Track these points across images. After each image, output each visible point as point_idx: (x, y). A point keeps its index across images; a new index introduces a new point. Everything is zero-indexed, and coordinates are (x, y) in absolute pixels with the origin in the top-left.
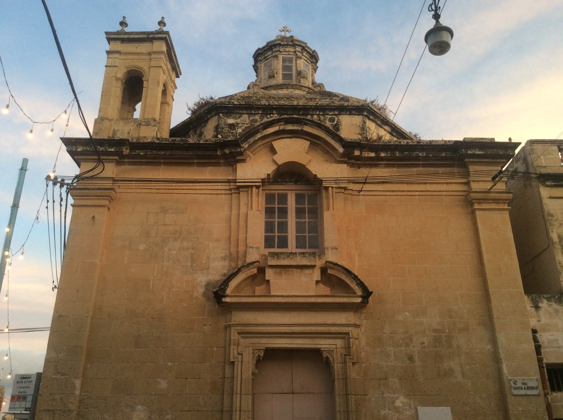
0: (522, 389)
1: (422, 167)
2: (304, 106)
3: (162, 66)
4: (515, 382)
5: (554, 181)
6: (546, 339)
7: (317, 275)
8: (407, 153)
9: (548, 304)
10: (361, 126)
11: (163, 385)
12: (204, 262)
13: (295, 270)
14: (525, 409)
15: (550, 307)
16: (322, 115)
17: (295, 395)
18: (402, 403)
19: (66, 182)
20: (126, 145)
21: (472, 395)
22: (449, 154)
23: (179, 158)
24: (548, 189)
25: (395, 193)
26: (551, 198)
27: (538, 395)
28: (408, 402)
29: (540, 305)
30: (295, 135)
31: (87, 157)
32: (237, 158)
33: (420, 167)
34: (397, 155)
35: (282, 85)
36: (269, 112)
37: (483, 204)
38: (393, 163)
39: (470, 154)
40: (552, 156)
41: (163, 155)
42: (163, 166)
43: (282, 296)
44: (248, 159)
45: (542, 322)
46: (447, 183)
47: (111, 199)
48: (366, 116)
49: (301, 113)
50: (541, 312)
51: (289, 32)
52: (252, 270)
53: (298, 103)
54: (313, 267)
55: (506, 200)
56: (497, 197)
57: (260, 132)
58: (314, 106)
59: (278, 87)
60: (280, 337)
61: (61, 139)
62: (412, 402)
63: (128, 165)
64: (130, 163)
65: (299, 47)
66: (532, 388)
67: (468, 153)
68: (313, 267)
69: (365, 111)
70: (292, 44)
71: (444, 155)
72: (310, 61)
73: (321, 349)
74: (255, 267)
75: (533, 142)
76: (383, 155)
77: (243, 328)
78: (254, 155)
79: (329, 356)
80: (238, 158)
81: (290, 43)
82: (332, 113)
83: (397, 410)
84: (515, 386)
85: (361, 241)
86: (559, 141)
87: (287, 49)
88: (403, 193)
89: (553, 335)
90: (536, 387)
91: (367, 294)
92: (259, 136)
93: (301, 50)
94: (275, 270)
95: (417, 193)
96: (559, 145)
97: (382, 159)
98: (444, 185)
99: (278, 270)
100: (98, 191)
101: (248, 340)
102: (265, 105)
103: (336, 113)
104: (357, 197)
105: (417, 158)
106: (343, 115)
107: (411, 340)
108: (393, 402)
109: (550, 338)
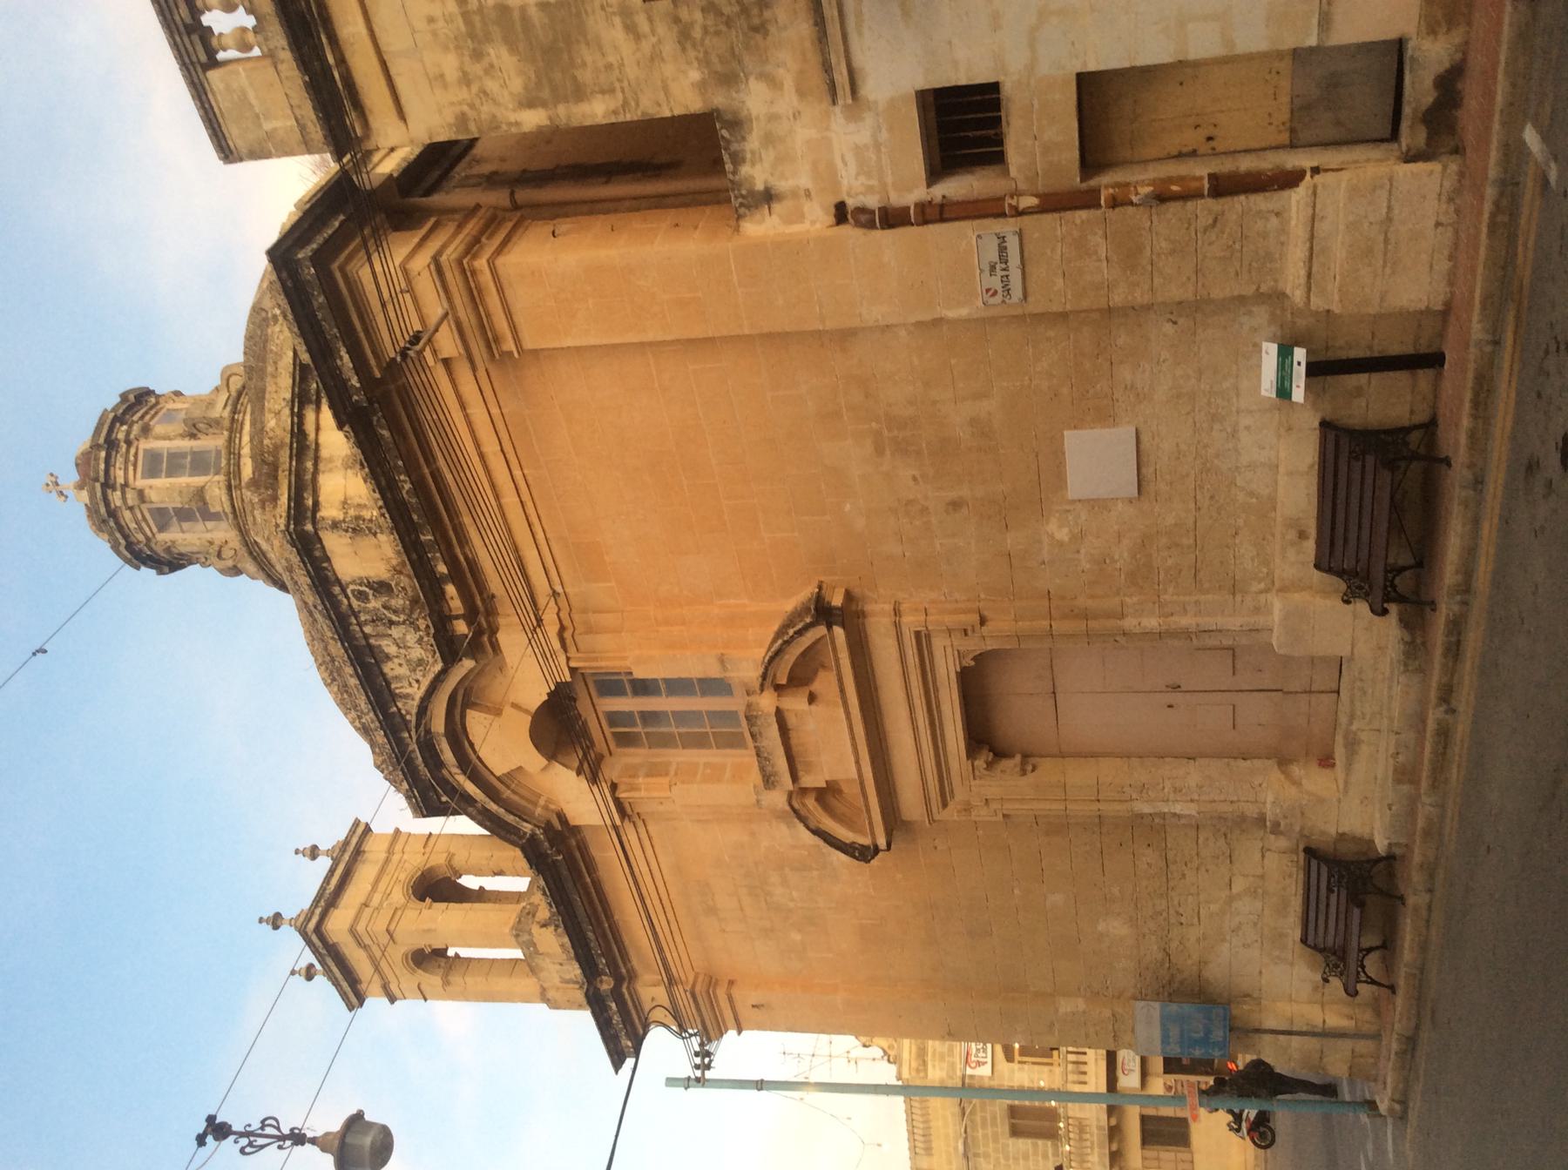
0: (1007, 276)
1: (435, 460)
3: (387, 930)
6: (856, 179)
7: (795, 704)
8: (415, 517)
9: (753, 164)
10: (349, 534)
11: (1057, 899)
14: (1060, 272)
15: (761, 159)
16: (357, 618)
18: (1060, 527)
19: (697, 1049)
20: (595, 988)
23: (591, 902)
24: (375, 123)
27: (1020, 234)
29: (760, 186)
32: (560, 828)
35: (255, 559)
36: (398, 719)
37: (497, 326)
38: (451, 533)
39: (360, 381)
40: (251, 95)
41: (595, 933)
42: (616, 917)
44: (552, 807)
47: (712, 982)
48: (314, 523)
49: (373, 661)
50: (781, 185)
54: (779, 713)
56: (465, 299)
61: (617, 1072)
63: (630, 962)
64: (625, 958)
66: (1002, 249)
67: (358, 385)
69: (303, 530)
71: (386, 433)
72: (128, 451)
73: (959, 670)
74: (804, 805)
76: (442, 568)
77: (934, 802)
78: (540, 796)
79: (971, 656)
82: (341, 597)
83: (1079, 537)
84: (1000, 291)
87: (133, 525)
88: (529, 505)
91: (822, 612)
92: (493, 807)
94: (801, 773)
95: (517, 473)
97: (452, 562)
98: (503, 501)
99: (799, 767)
100: (703, 1009)
102: (386, 735)
103: (337, 590)
105: (419, 487)
106: (335, 574)
107: (909, 502)
108: (1061, 544)
109: (853, 167)
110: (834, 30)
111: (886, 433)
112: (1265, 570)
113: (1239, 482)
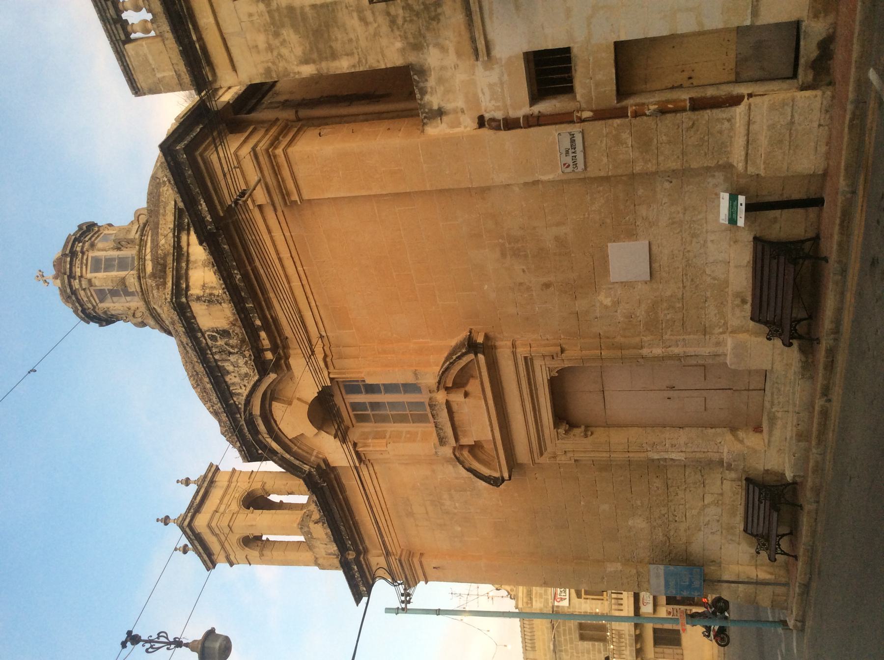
2: (208, 376)
4: (566, 166)
5: (200, 68)
7: (457, 398)
8: (243, 294)
9: (432, 94)
11: (605, 507)
12: (463, 481)
13: (456, 419)
17: (606, 389)
18: (606, 297)
21: (589, 215)
22: (221, 239)
25: (305, 282)
26: (234, 68)
27: (583, 133)
28: (604, 291)
29: (435, 107)
30: (269, 415)
31: (358, 539)
33: (255, 266)
34: (251, 305)
39: (211, 218)
40: (150, 58)
43: (492, 431)
44: (321, 456)
45: (464, 107)
46: (269, 232)
47: (411, 554)
48: (187, 297)
49: (220, 374)
50: (448, 106)
51: (43, 273)
52: (466, 456)
53: (208, 383)
54: (448, 404)
55: (269, 156)
57: (282, 456)
58: (203, 365)
59: (159, 320)
60: (540, 418)
62: (604, 287)
65: (73, 284)
66: (573, 141)
68: (448, 404)
70: (73, 296)
71: (226, 247)
75: (135, 90)
76: (258, 322)
80: (324, 467)
81: (74, 298)
83: (616, 303)
84: (571, 166)
85: (395, 335)
86: (112, 43)
87: (85, 299)
89: (482, 90)
90: (572, 136)
91: (471, 346)
92: (287, 456)
93: (75, 279)
95: (300, 269)
96: (120, 43)
97: (263, 318)
100: (406, 570)
101: (548, 442)
102: (227, 416)
103: (199, 335)
104: (330, 338)
105: (245, 277)
106: (198, 326)
107: (521, 284)
108: (606, 307)
110: (477, 18)
111: (507, 245)
112: (723, 321)
113: (708, 271)
